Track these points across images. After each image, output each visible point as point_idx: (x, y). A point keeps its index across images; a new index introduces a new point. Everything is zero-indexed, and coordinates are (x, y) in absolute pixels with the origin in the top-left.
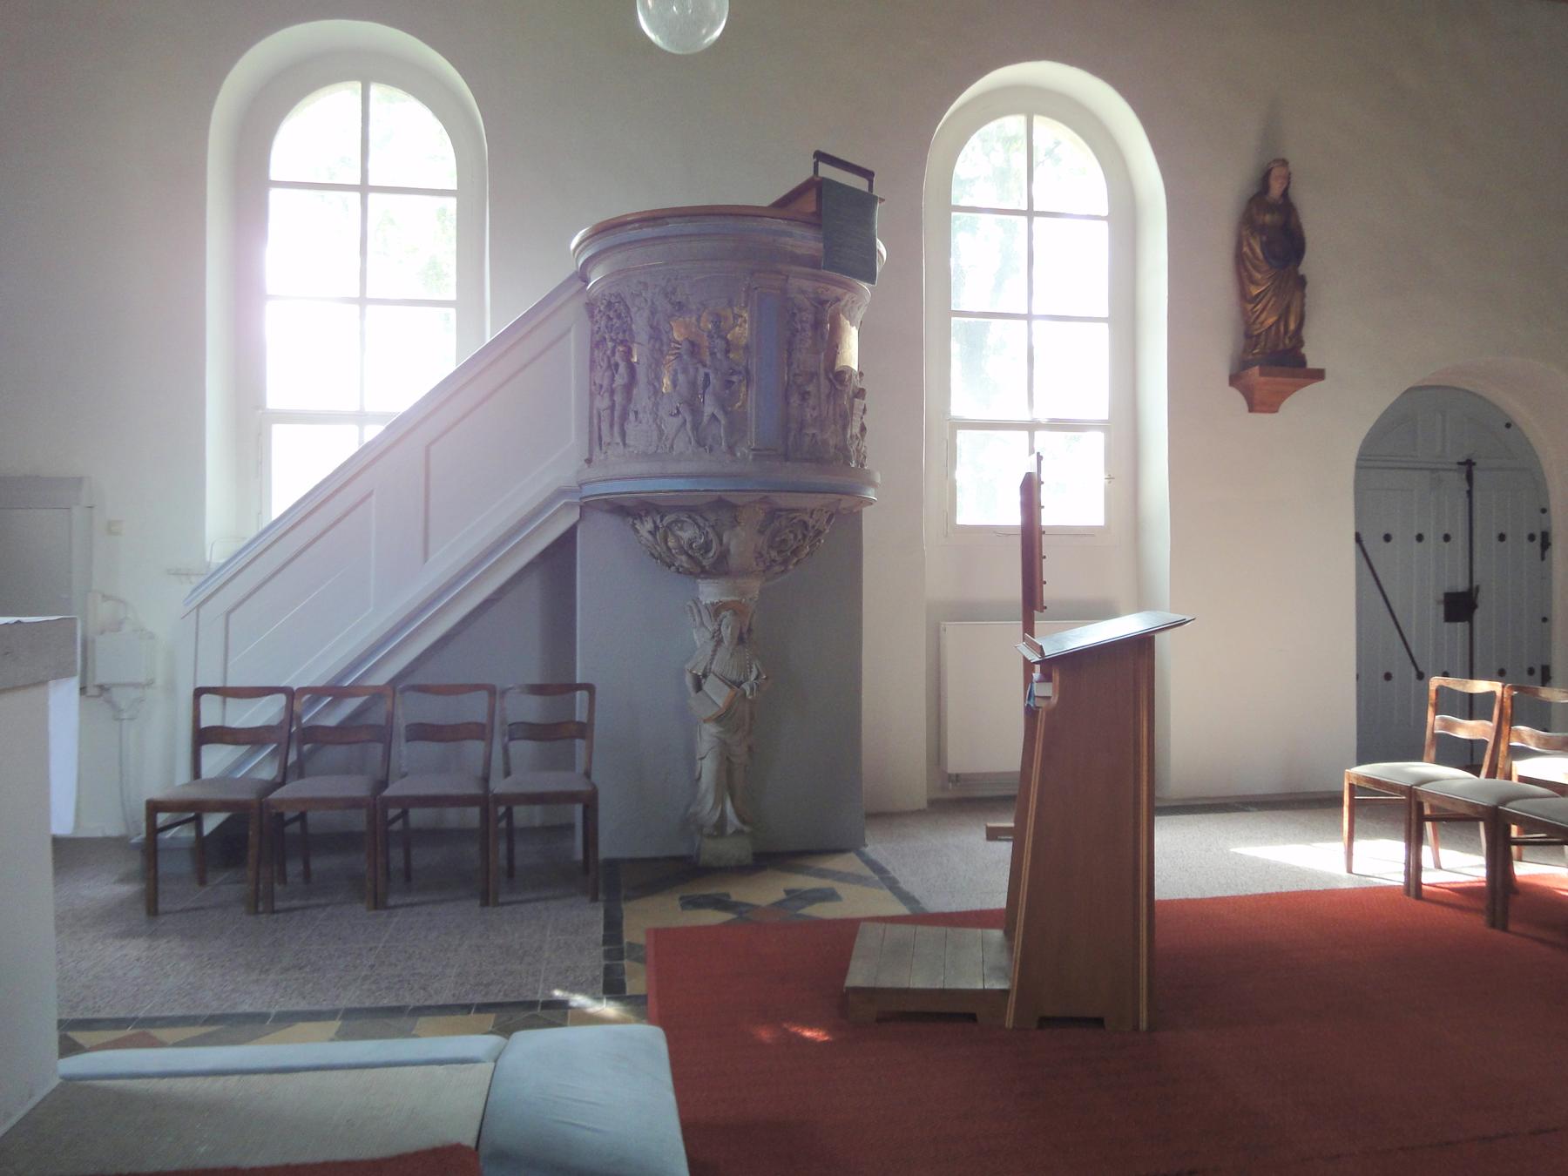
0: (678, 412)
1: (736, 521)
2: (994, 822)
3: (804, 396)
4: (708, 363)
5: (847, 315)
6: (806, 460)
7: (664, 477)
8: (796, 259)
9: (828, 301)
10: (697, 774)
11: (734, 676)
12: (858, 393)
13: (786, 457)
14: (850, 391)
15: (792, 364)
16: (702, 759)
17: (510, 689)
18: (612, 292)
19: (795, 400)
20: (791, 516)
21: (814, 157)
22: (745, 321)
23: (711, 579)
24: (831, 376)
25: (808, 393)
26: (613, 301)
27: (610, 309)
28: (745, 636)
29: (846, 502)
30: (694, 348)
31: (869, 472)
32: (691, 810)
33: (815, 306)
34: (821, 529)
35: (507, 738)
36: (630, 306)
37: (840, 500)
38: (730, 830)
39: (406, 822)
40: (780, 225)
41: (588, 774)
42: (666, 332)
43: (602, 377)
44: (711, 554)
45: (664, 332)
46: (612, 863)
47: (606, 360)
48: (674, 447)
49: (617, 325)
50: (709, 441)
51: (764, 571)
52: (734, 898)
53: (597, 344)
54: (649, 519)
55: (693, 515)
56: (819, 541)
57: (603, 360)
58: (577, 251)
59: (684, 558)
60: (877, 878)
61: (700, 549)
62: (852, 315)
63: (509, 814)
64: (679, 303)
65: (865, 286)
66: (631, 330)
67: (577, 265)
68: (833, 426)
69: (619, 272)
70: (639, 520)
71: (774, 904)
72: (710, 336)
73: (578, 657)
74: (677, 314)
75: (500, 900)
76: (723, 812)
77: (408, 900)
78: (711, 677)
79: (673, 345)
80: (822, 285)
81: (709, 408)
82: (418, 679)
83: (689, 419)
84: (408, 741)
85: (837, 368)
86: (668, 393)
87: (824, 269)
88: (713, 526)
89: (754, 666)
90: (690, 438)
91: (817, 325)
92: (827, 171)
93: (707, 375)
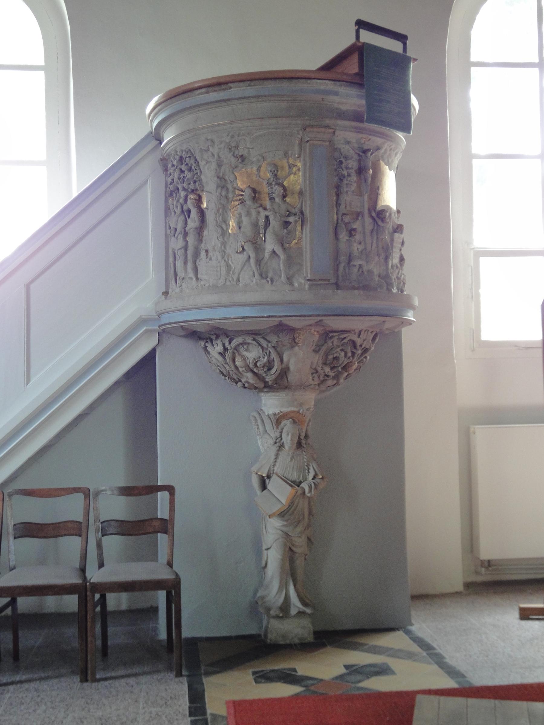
0: (243, 249)
1: (295, 342)
2: (525, 603)
3: (351, 232)
4: (268, 207)
5: (386, 161)
6: (354, 288)
7: (232, 306)
8: (341, 115)
9: (369, 150)
10: (263, 564)
11: (294, 476)
12: (397, 228)
13: (337, 286)
14: (390, 227)
15: (340, 205)
16: (267, 549)
17: (102, 491)
18: (184, 148)
19: (343, 236)
20: (343, 336)
21: (355, 25)
22: (299, 170)
23: (273, 392)
24: (374, 214)
25: (355, 230)
26: (184, 156)
27: (182, 164)
28: (303, 442)
29: (390, 323)
30: (255, 193)
31: (409, 297)
32: (258, 595)
33: (359, 155)
34: (367, 347)
35: (100, 534)
36: (199, 160)
37: (384, 322)
38: (293, 612)
39: (14, 609)
40: (328, 85)
41: (170, 564)
42: (231, 182)
43: (177, 222)
44: (273, 371)
45: (229, 182)
46: (193, 642)
47: (179, 207)
48: (240, 280)
49: (188, 177)
50: (270, 275)
51: (319, 385)
52: (300, 672)
53: (171, 194)
54: (219, 342)
55: (256, 337)
56: (366, 357)
57: (177, 207)
58: (152, 115)
59: (249, 375)
60: (424, 654)
61: (263, 367)
62: (390, 161)
63: (103, 597)
64: (242, 156)
65: (401, 135)
66: (200, 180)
67: (152, 127)
68: (377, 258)
69: (183, 133)
70: (210, 343)
71: (337, 678)
72: (269, 184)
73: (159, 460)
74: (240, 165)
75: (98, 676)
76: (287, 598)
77: (18, 678)
78: (274, 477)
79: (237, 192)
80: (364, 136)
81: (270, 245)
82: (22, 484)
83: (253, 255)
84: (15, 538)
85: (379, 208)
86: (234, 234)
87: (367, 122)
88: (274, 347)
89: (311, 468)
90: (254, 272)
91: (361, 171)
92: (367, 37)
93: (267, 217)
